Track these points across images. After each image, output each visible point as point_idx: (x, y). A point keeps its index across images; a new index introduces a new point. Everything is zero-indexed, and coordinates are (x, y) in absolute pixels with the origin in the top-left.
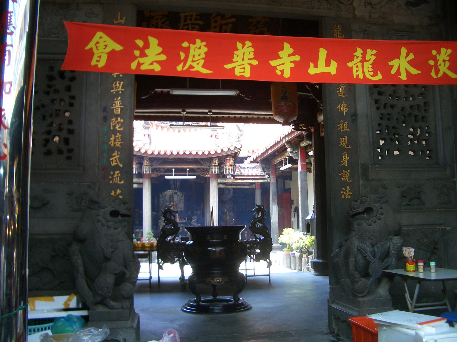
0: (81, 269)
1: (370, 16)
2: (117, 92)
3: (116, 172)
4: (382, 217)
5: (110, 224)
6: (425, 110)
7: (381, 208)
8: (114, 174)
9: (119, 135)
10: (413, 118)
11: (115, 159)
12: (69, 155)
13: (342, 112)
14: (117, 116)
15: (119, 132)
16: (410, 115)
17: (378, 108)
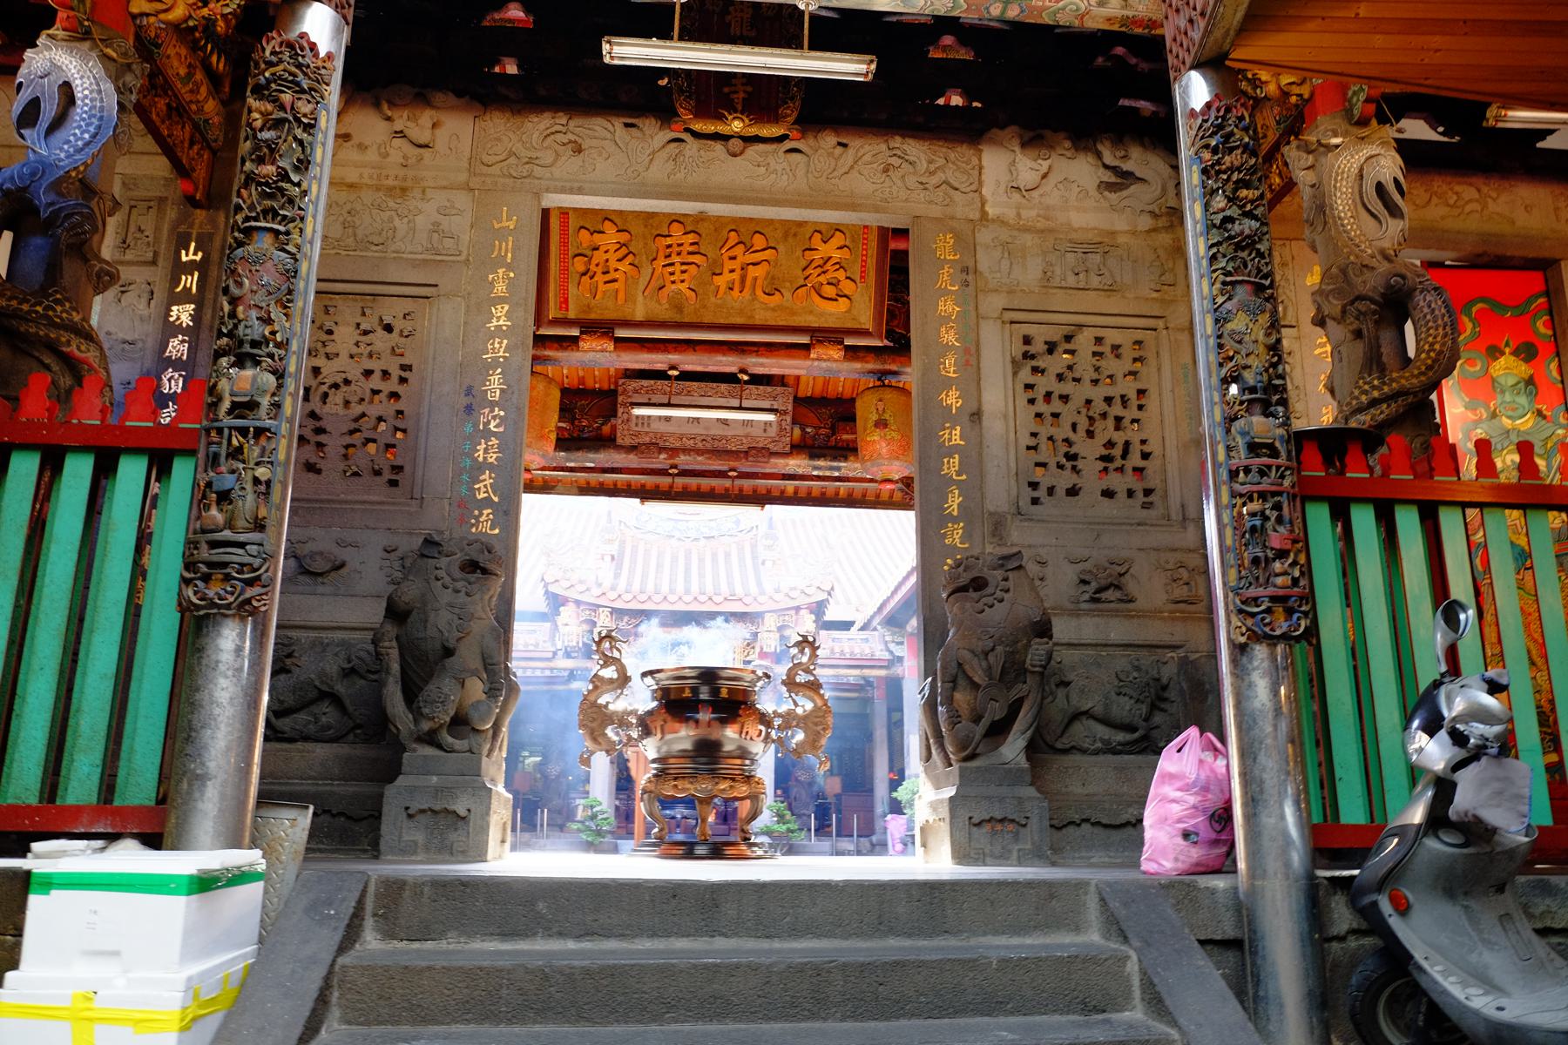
0: (395, 667)
1: (1019, 215)
2: (495, 359)
3: (485, 512)
4: (1006, 596)
5: (459, 585)
6: (1140, 407)
7: (1006, 579)
8: (481, 514)
9: (494, 441)
10: (1110, 423)
11: (484, 487)
12: (394, 477)
13: (949, 407)
14: (492, 405)
15: (495, 434)
16: (1104, 415)
17: (1032, 401)
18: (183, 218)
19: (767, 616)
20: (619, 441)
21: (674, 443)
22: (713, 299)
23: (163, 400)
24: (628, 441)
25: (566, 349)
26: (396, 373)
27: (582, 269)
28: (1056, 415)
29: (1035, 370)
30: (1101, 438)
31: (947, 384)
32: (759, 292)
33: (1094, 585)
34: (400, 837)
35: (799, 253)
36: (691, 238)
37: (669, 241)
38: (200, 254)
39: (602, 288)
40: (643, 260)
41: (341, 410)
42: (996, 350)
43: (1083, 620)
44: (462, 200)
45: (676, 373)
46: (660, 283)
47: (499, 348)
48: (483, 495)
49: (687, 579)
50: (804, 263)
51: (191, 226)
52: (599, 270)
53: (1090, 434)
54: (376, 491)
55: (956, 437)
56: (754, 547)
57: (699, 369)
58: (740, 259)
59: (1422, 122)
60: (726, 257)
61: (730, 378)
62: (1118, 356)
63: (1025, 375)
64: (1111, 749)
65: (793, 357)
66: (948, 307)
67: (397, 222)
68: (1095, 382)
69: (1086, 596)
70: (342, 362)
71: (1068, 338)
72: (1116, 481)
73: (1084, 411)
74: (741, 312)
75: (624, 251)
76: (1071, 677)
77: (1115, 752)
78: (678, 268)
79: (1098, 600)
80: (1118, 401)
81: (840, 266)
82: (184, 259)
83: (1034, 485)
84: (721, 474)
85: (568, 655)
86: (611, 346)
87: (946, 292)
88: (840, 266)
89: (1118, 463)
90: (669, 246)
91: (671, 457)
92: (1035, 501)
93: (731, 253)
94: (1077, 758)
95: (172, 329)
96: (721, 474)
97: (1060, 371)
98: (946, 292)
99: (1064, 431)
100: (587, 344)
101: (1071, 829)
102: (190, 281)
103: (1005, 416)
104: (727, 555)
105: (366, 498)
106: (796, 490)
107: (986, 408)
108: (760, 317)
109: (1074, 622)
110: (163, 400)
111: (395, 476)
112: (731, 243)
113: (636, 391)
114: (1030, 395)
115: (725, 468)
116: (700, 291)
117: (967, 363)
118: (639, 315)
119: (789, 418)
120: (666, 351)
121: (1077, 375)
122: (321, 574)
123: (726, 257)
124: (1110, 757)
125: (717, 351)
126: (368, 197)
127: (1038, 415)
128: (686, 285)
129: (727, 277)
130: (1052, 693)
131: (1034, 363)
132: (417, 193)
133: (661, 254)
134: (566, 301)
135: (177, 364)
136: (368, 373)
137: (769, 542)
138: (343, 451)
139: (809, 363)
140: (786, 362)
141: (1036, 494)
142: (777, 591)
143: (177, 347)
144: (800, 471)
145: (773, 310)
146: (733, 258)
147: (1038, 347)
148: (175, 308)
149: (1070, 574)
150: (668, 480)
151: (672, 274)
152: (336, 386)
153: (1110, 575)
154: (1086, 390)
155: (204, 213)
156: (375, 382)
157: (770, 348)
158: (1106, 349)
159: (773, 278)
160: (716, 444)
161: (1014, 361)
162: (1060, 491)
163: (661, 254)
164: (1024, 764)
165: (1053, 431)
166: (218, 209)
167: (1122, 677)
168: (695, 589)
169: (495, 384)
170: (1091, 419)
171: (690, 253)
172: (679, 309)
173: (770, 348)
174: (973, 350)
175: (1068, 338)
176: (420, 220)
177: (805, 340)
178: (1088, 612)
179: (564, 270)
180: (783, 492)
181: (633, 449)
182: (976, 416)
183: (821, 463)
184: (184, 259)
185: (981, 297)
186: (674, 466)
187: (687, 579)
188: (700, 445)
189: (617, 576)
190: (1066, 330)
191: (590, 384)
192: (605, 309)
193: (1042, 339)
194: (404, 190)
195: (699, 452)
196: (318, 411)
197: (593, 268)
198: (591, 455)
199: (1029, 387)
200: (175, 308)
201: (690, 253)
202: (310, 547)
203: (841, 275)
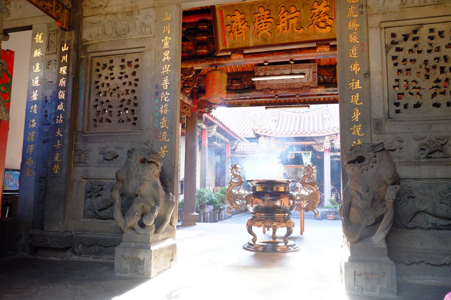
3: (164, 133)
8: (162, 134)
9: (166, 105)
10: (438, 70)
11: (164, 123)
15: (166, 102)
16: (434, 67)
17: (396, 65)
18: (63, 36)
19: (326, 137)
20: (257, 88)
21: (275, 87)
22: (278, 35)
23: (59, 102)
24: (260, 88)
25: (227, 60)
26: (133, 82)
27: (229, 30)
28: (408, 70)
29: (398, 50)
30: (433, 78)
31: (353, 61)
32: (295, 29)
33: (428, 151)
34: (121, 266)
35: (309, 11)
36: (267, 12)
37: (259, 15)
38: (67, 48)
39: (237, 36)
40: (250, 23)
41: (117, 99)
42: (376, 41)
43: (422, 167)
44: (152, 12)
45: (267, 64)
46: (258, 31)
47: (166, 68)
48: (163, 127)
49: (299, 127)
50: (311, 15)
51: (64, 38)
52: (235, 30)
53: (428, 77)
54: (127, 127)
55: (357, 85)
56: (322, 114)
57: (275, 61)
58: (286, 17)
59: (349, 254)
60: (281, 17)
61: (288, 63)
62: (442, 37)
63: (393, 52)
64: (436, 227)
65: (310, 52)
66: (353, 25)
67: (130, 25)
68: (429, 51)
69: (424, 156)
70: (116, 80)
71: (415, 32)
72: (439, 99)
73: (424, 66)
74: (288, 38)
75: (243, 21)
76: (415, 194)
77: (439, 229)
78: (263, 24)
79: (430, 158)
80: (442, 59)
81: (326, 14)
82: (63, 50)
83: (397, 104)
84: (294, 96)
85: (234, 167)
86: (242, 57)
87: (352, 18)
88: (326, 14)
89: (442, 90)
90: (259, 17)
91: (275, 92)
92: (398, 112)
93: (282, 16)
94: (418, 231)
95: (60, 76)
96: (294, 96)
97: (411, 48)
98: (352, 18)
99: (414, 76)
100: (234, 57)
101: (415, 265)
102: (65, 58)
103: (382, 73)
104: (314, 117)
105: (125, 130)
106: (324, 99)
107: (372, 70)
108: (296, 39)
109: (417, 168)
110: (59, 102)
111: (135, 121)
112: (282, 12)
113: (261, 70)
114: (395, 61)
115: (295, 94)
116: (272, 32)
117: (363, 50)
118: (251, 45)
119: (316, 74)
120: (262, 56)
121: (420, 49)
122: (110, 160)
123: (281, 17)
124: (436, 231)
125: (281, 54)
126: (120, 16)
127: (400, 71)
128: (267, 30)
129: (282, 25)
130: (405, 201)
131: (397, 46)
132: (136, 12)
133: (257, 20)
134: (225, 43)
135: (62, 88)
136: (125, 83)
137: (327, 112)
138: (118, 113)
139: (316, 54)
140: (307, 55)
141: (398, 108)
142: (329, 129)
143: (62, 82)
144: (322, 93)
145: (301, 35)
146: (283, 18)
147: (400, 37)
148: (61, 68)
149: (415, 145)
150: (275, 99)
151: (261, 27)
152: (115, 90)
153: (437, 146)
154: (425, 56)
155: (68, 32)
156: (127, 87)
157: (301, 50)
158: (436, 34)
159: (300, 23)
160: (291, 86)
161: (386, 46)
162: (411, 106)
163: (257, 20)
164: (385, 246)
165: (407, 77)
166: (72, 30)
167: (443, 195)
168: (301, 130)
169: (166, 83)
170: (428, 70)
171: (267, 18)
172: (265, 40)
173: (301, 50)
174: (365, 44)
175: (415, 32)
176: (138, 22)
177: (314, 45)
178: (424, 164)
179: (224, 31)
180: (319, 99)
181: (261, 91)
182: (367, 74)
183: (330, 89)
184: (63, 50)
185: (369, 18)
186: (277, 95)
187: (299, 127)
188: (285, 87)
189: (277, 126)
190: (414, 28)
191: (246, 69)
192: (239, 44)
193: (401, 34)
194: (132, 12)
195: (285, 90)
196: (109, 100)
197: (233, 29)
198: (248, 94)
199: (394, 58)
200: (61, 68)
201: (267, 18)
202: (107, 150)
203: (326, 17)
